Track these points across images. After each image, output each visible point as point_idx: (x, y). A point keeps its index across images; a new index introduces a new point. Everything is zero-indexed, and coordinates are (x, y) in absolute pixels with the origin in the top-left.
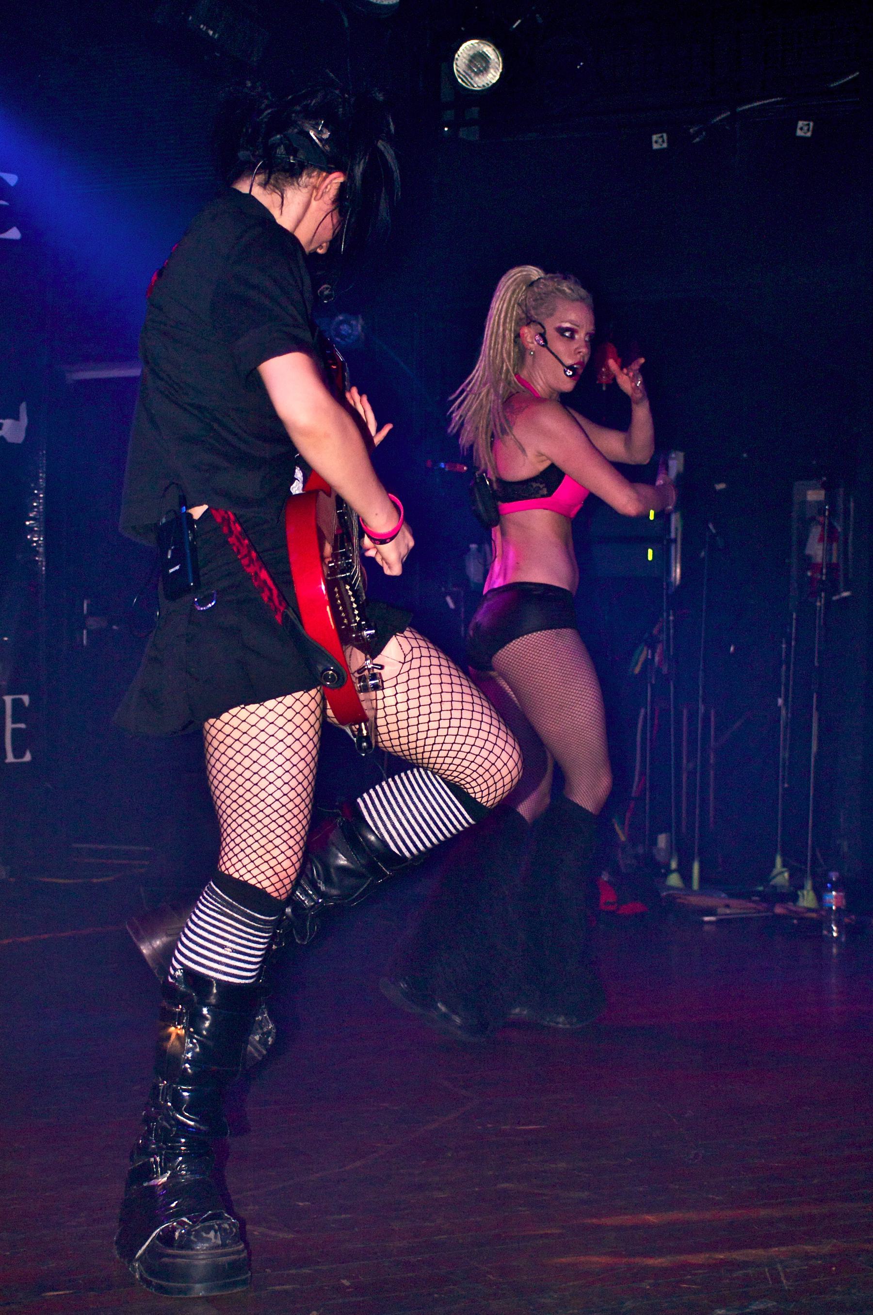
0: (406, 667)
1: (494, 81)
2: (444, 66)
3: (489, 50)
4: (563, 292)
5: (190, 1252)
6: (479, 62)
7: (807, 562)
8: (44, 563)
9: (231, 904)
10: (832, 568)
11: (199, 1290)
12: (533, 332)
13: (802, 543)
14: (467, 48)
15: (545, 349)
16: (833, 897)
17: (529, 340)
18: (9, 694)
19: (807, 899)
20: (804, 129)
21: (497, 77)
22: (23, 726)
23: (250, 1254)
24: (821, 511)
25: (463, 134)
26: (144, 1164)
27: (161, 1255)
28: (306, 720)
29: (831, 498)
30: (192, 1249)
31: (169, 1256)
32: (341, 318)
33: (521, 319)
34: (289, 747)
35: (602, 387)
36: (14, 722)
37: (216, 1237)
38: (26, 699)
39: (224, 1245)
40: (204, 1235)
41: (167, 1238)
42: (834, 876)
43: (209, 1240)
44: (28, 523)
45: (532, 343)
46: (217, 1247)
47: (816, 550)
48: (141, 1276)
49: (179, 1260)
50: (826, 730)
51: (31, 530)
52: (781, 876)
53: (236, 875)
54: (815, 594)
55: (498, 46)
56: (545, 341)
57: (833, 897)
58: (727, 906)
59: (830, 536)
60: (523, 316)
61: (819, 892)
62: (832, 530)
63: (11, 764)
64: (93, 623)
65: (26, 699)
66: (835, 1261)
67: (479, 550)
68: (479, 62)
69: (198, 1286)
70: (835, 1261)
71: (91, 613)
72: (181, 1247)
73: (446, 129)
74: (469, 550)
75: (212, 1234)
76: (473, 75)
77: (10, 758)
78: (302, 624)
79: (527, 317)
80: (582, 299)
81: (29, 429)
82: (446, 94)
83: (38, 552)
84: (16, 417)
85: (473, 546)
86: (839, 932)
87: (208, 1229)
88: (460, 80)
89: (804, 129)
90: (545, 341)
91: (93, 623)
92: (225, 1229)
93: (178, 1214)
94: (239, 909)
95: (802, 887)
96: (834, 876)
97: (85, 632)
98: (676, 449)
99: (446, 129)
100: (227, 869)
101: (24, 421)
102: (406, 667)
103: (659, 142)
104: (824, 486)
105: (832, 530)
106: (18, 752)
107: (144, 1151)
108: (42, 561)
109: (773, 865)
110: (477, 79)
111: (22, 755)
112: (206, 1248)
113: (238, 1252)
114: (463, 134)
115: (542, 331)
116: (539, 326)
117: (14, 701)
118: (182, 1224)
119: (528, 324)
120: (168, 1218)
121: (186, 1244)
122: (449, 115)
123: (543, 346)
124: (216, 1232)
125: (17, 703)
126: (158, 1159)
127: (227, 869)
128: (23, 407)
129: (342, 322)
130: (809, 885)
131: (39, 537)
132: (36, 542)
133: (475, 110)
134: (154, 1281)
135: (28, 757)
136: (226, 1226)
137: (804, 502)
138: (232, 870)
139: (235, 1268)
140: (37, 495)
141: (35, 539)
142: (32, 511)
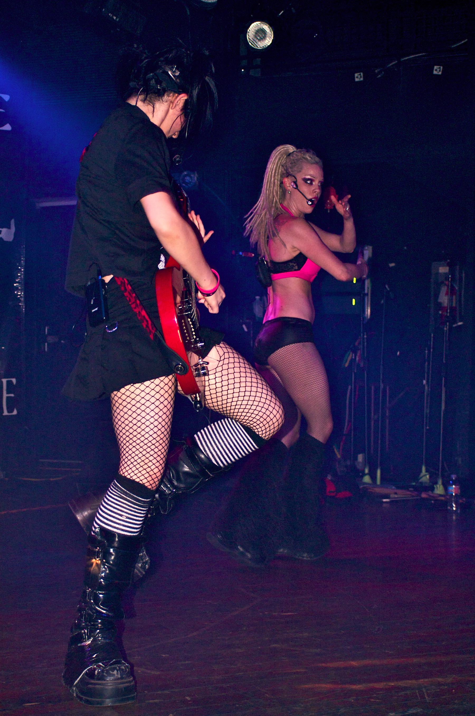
0: (221, 363)
1: (269, 44)
2: (241, 36)
3: (266, 27)
4: (306, 159)
5: (104, 682)
6: (261, 34)
7: (439, 306)
8: (24, 307)
9: (126, 492)
10: (453, 309)
11: (108, 702)
12: (290, 181)
13: (437, 296)
14: (254, 26)
15: (297, 190)
16: (453, 489)
17: (288, 185)
18: (5, 378)
19: (439, 490)
20: (437, 70)
21: (271, 42)
22: (12, 395)
23: (136, 683)
24: (447, 278)
25: (252, 73)
26: (78, 634)
27: (88, 684)
28: (166, 392)
29: (452, 271)
30: (105, 680)
31: (92, 684)
32: (185, 173)
33: (283, 174)
34: (157, 407)
35: (327, 211)
36: (7, 393)
37: (117, 674)
38: (14, 380)
39: (122, 678)
40: (111, 672)
41: (91, 674)
42: (454, 477)
43: (114, 675)
44: (15, 285)
45: (290, 187)
46: (118, 679)
47: (444, 299)
48: (77, 695)
49: (97, 686)
50: (449, 397)
51: (17, 288)
52: (425, 477)
53: (129, 477)
54: (443, 324)
55: (271, 25)
56: (297, 185)
57: (453, 489)
58: (396, 493)
59: (452, 292)
60: (285, 172)
61: (446, 486)
62: (453, 288)
63: (6, 416)
64: (51, 339)
65: (14, 380)
66: (454, 686)
67: (261, 300)
68: (261, 34)
69: (108, 700)
70: (454, 686)
71: (49, 334)
72: (99, 679)
73: (243, 70)
74: (255, 299)
75: (115, 672)
76: (257, 41)
77: (6, 413)
78: (164, 340)
79: (287, 173)
80: (317, 163)
81: (16, 234)
82: (243, 51)
83: (21, 300)
84: (9, 227)
85: (258, 298)
86: (456, 507)
87: (113, 669)
88: (250, 44)
89: (437, 70)
90: (297, 185)
91: (51, 339)
92: (123, 669)
93: (97, 661)
94: (130, 495)
95: (436, 483)
96: (454, 477)
97: (46, 344)
98: (368, 245)
99: (243, 70)
100: (124, 473)
101: (13, 229)
102: (221, 363)
103: (358, 77)
104: (448, 265)
105: (453, 288)
106: (10, 409)
107: (78, 627)
108: (23, 306)
109: (421, 471)
110: (259, 43)
111: (12, 411)
112: (112, 680)
113: (130, 682)
114: (252, 73)
115: (295, 180)
116: (293, 178)
117: (8, 382)
118: (99, 666)
119: (287, 177)
120: (91, 663)
121: (101, 677)
122: (244, 62)
123: (295, 188)
124: (117, 671)
125: (9, 383)
126: (86, 631)
127: (124, 473)
128: (13, 222)
129: (186, 176)
130: (440, 482)
131: (21, 292)
132: (19, 295)
133: (259, 60)
134: (84, 697)
135: (15, 412)
136: (123, 667)
137: (438, 273)
138: (126, 474)
139: (128, 690)
140: (20, 269)
141: (19, 294)
142: (17, 278)
